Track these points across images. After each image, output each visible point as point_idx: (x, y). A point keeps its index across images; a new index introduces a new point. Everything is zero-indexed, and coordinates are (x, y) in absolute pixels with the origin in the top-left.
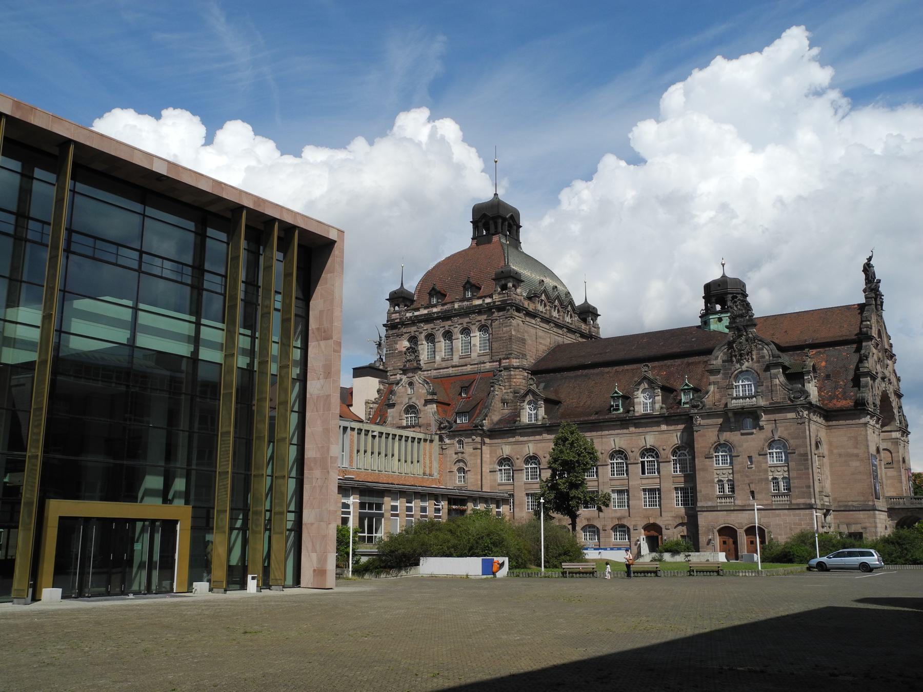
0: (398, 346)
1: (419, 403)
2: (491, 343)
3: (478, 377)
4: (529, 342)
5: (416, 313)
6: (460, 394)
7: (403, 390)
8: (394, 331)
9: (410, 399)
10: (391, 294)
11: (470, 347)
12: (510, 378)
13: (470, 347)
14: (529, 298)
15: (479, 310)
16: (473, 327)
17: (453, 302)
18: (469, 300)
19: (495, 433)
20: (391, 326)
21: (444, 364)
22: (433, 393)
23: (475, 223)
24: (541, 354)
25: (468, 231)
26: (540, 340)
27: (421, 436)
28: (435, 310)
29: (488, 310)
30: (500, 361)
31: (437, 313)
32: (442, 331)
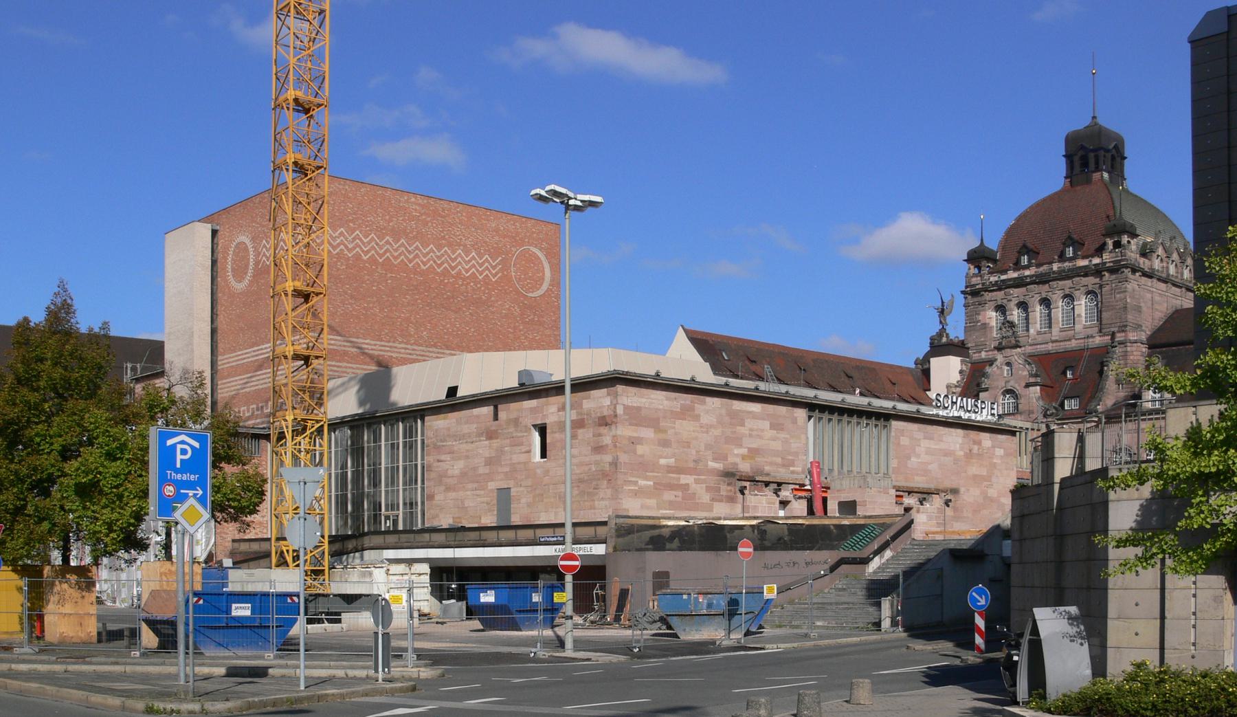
0: (980, 318)
1: (1019, 389)
2: (1100, 312)
3: (1086, 354)
4: (1144, 309)
5: (1003, 277)
6: (1064, 373)
7: (998, 372)
8: (976, 299)
9: (1007, 382)
10: (969, 254)
11: (1070, 319)
12: (1125, 355)
13: (1070, 319)
14: (1144, 254)
15: (1085, 272)
16: (1077, 293)
17: (1051, 263)
18: (1070, 259)
19: (1112, 417)
20: (973, 293)
21: (1040, 339)
22: (1036, 376)
23: (1069, 157)
24: (1158, 323)
25: (1061, 166)
26: (1156, 306)
27: (1028, 425)
28: (1027, 273)
29: (1098, 272)
30: (1113, 335)
31: (1031, 276)
32: (1038, 297)
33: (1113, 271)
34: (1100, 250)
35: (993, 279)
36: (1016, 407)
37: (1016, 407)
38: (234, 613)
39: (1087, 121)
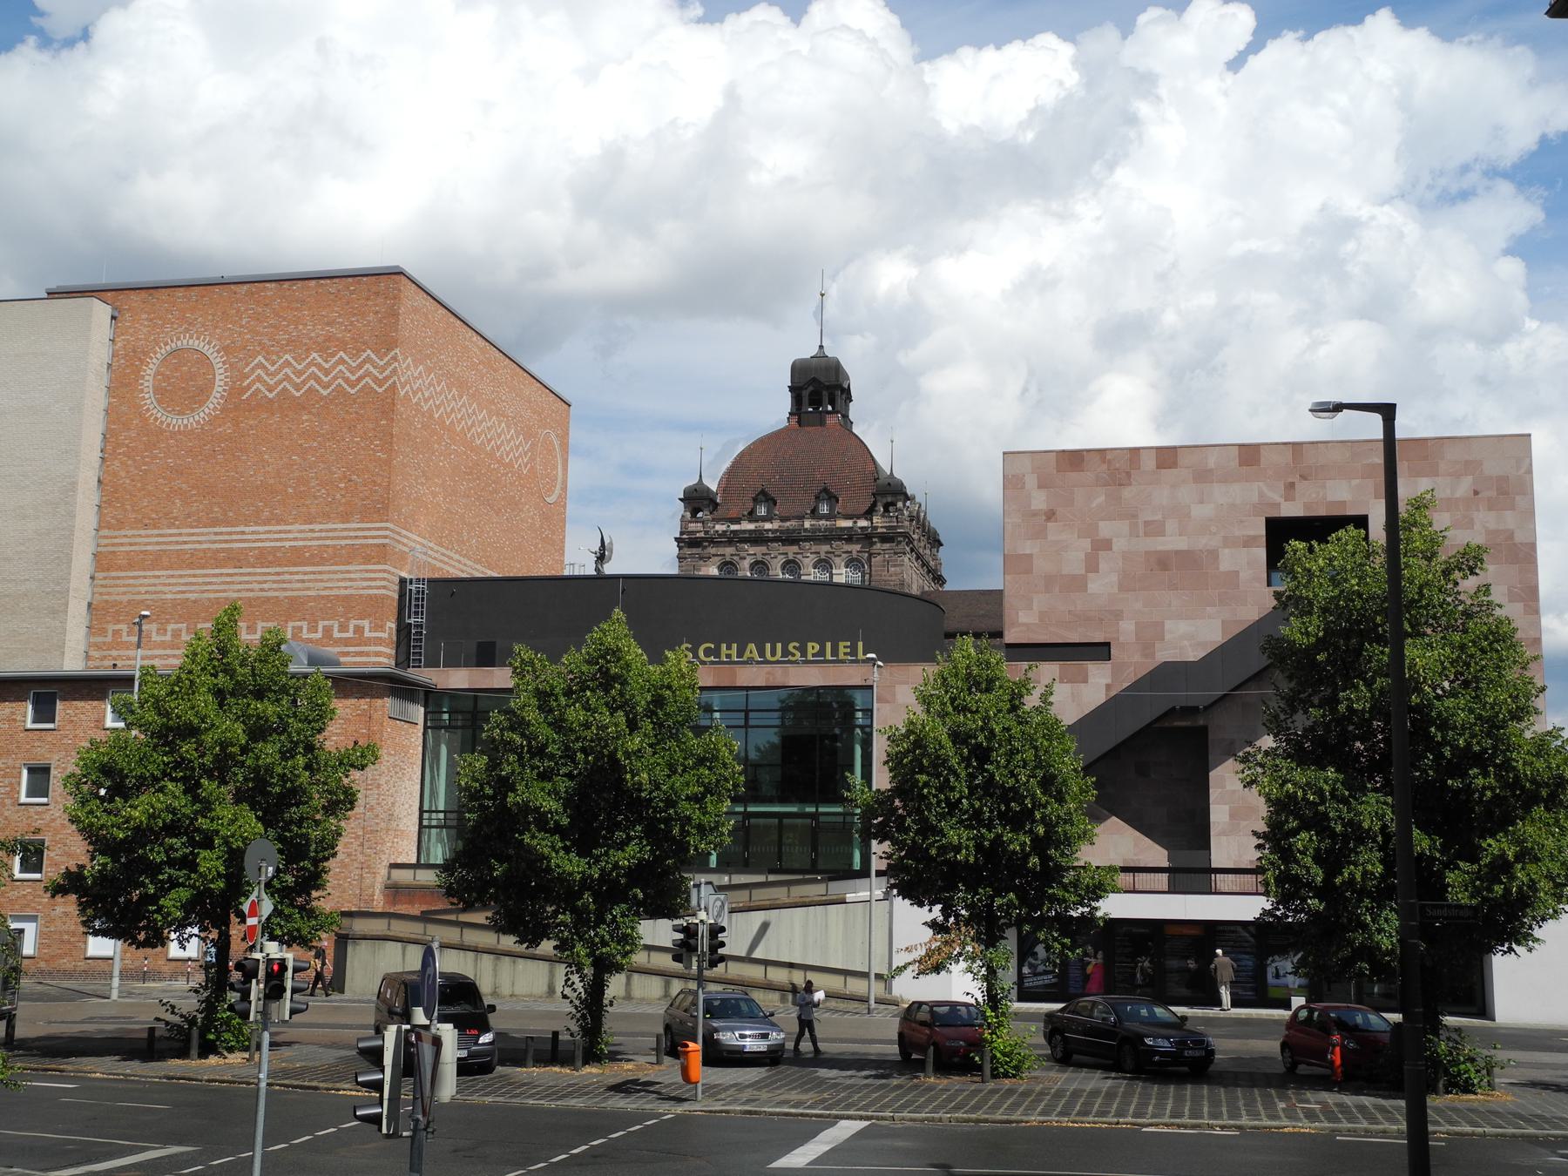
5: (734, 527)
15: (849, 536)
17: (801, 518)
25: (785, 403)
28: (768, 526)
29: (867, 537)
33: (885, 539)
34: (869, 514)
35: (720, 528)
36: (814, 862)
37: (814, 862)
38: (91, 952)
39: (814, 351)
